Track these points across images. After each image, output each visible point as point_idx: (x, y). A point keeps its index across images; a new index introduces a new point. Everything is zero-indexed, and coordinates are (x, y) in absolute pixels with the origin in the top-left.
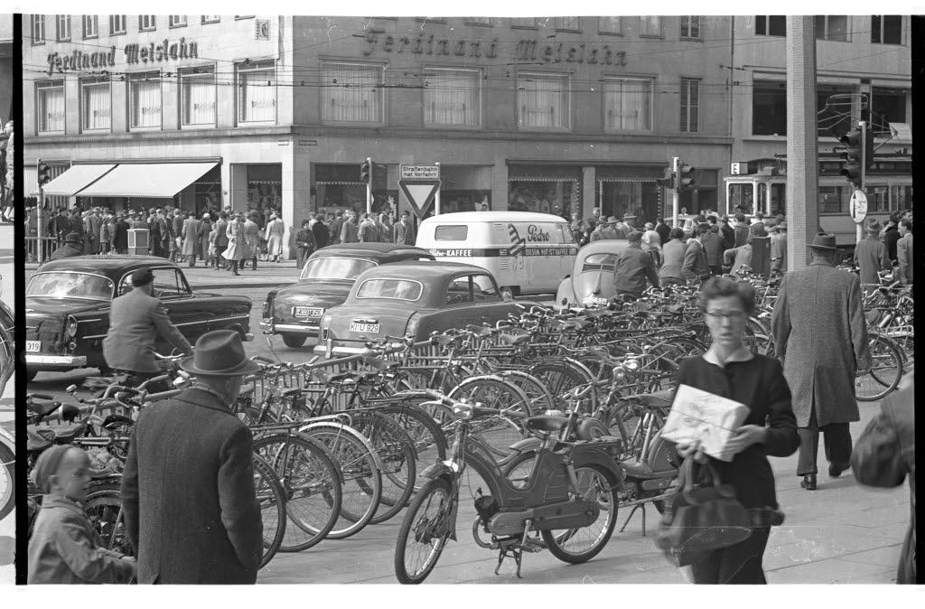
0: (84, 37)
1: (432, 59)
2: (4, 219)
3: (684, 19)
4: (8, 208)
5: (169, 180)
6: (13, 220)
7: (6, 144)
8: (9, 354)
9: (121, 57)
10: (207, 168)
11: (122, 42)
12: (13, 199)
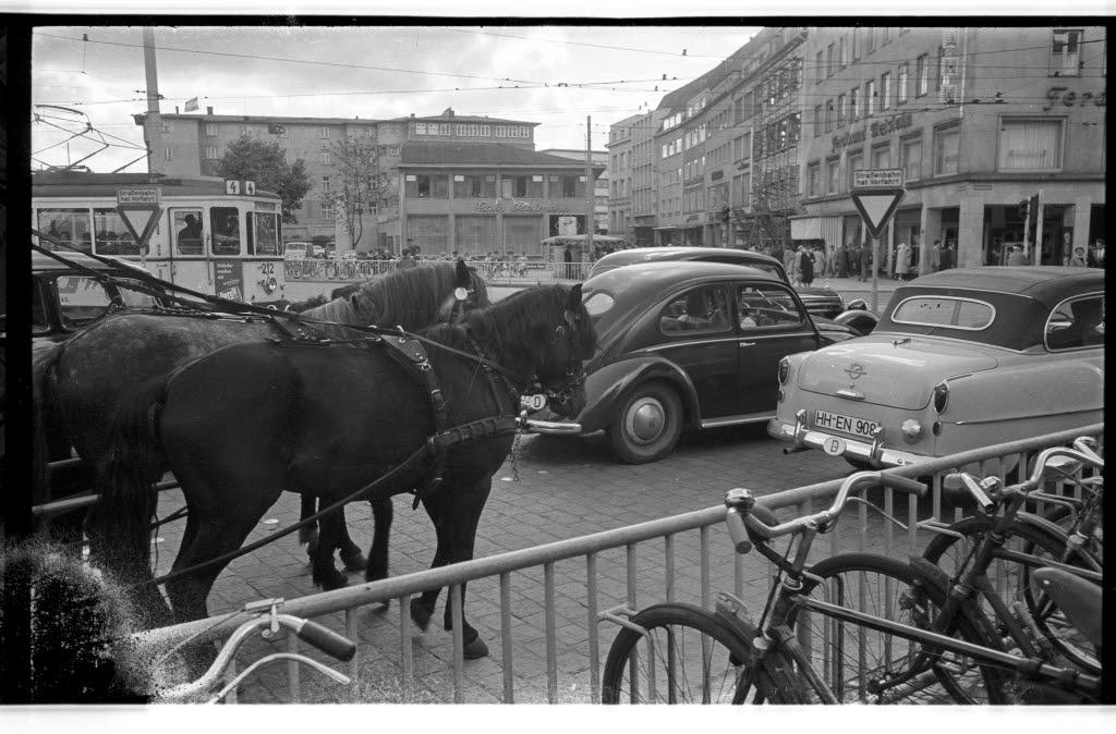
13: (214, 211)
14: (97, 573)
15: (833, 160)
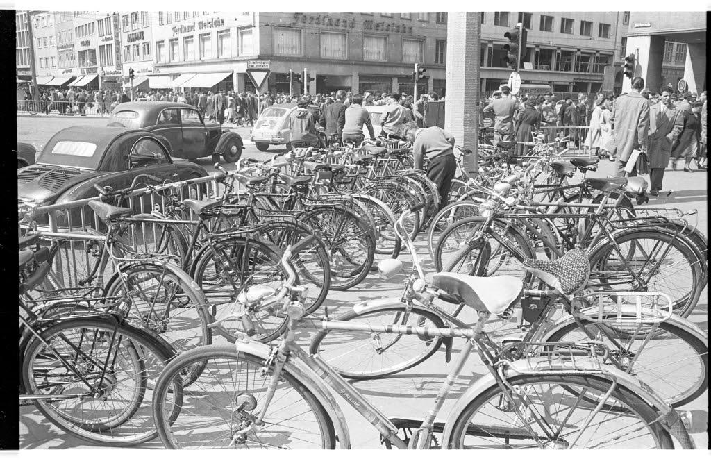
0: (185, 19)
1: (325, 27)
2: (699, 167)
3: (438, 14)
4: (703, 158)
5: (210, 81)
6: (706, 167)
7: (701, 109)
8: (703, 271)
9: (197, 27)
10: (228, 75)
11: (197, 20)
12: (706, 151)
13: (140, 213)
14: (512, 55)
15: (173, 42)
